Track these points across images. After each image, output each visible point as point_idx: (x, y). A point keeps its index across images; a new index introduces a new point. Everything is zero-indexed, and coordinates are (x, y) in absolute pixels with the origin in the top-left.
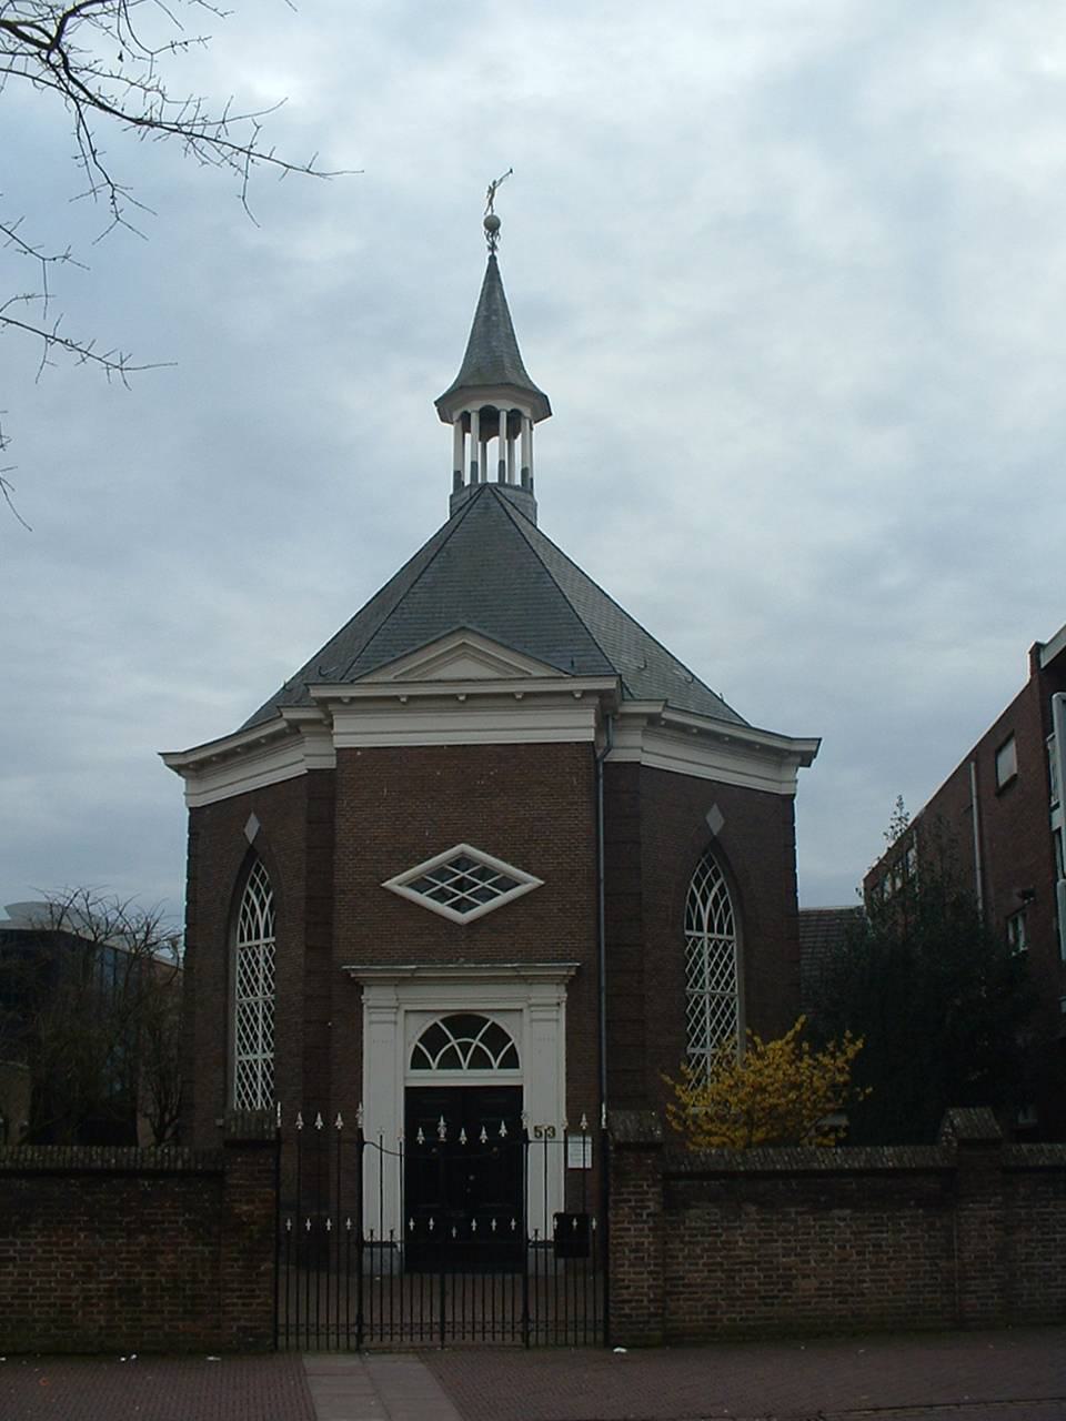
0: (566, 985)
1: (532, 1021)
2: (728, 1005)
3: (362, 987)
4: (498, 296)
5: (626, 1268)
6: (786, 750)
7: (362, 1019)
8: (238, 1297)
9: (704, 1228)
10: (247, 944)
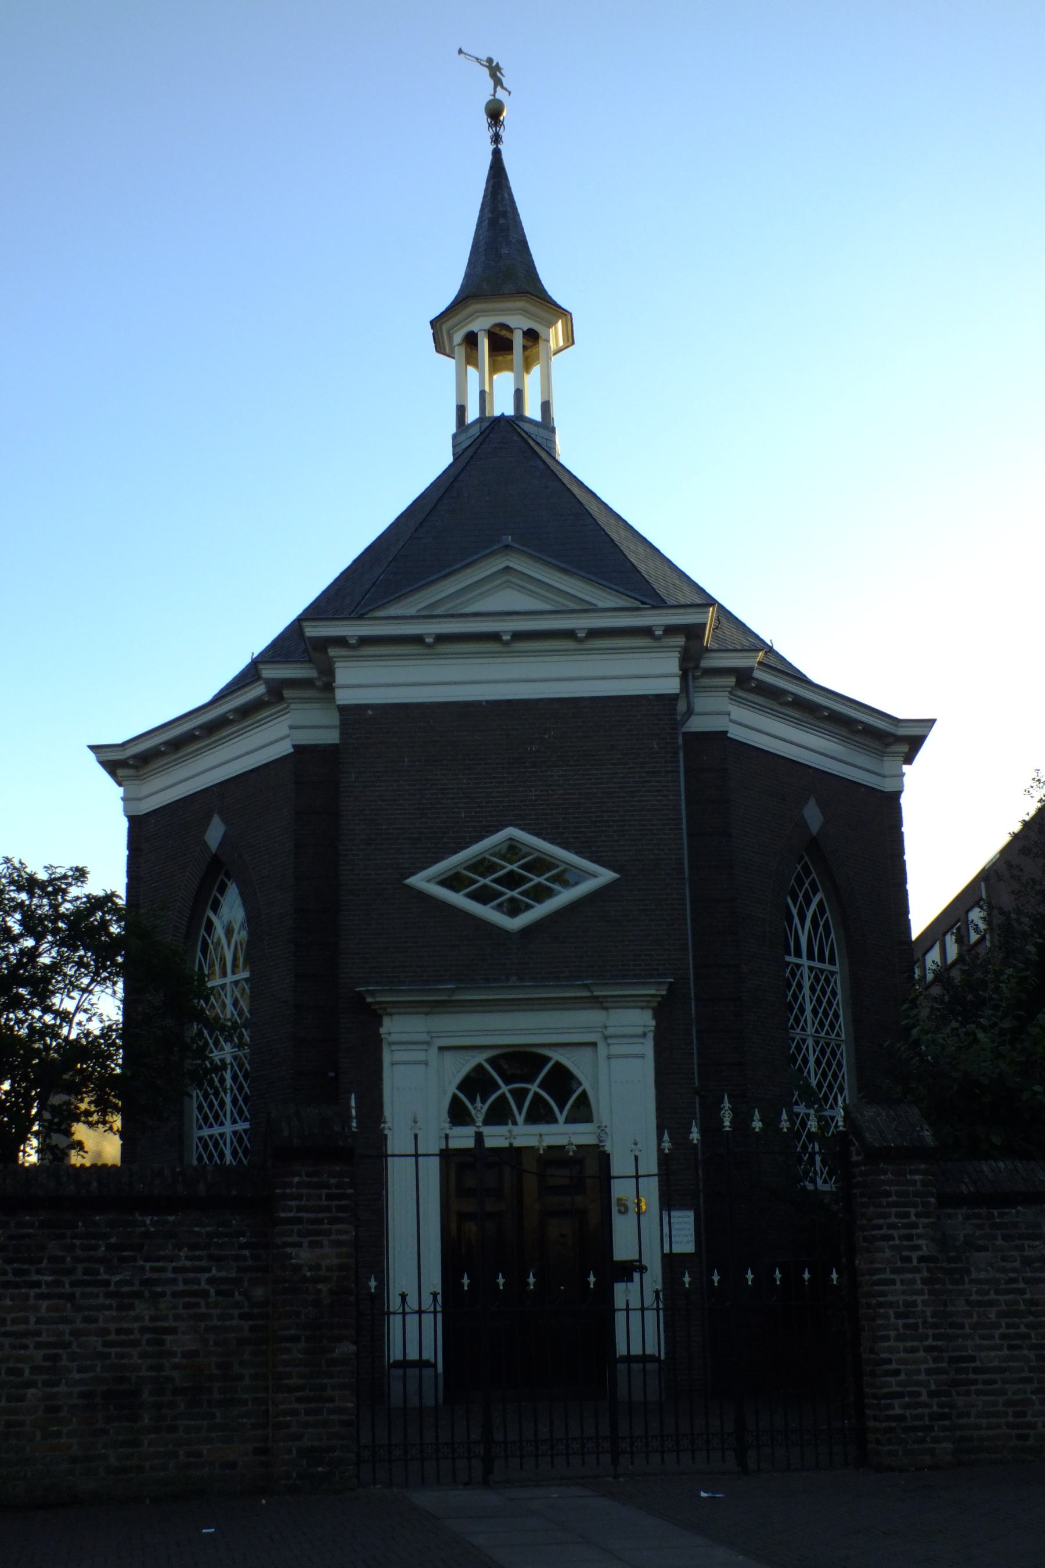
0: (653, 1009)
1: (609, 1058)
2: (834, 1054)
5: (892, 1343)
8: (299, 1400)
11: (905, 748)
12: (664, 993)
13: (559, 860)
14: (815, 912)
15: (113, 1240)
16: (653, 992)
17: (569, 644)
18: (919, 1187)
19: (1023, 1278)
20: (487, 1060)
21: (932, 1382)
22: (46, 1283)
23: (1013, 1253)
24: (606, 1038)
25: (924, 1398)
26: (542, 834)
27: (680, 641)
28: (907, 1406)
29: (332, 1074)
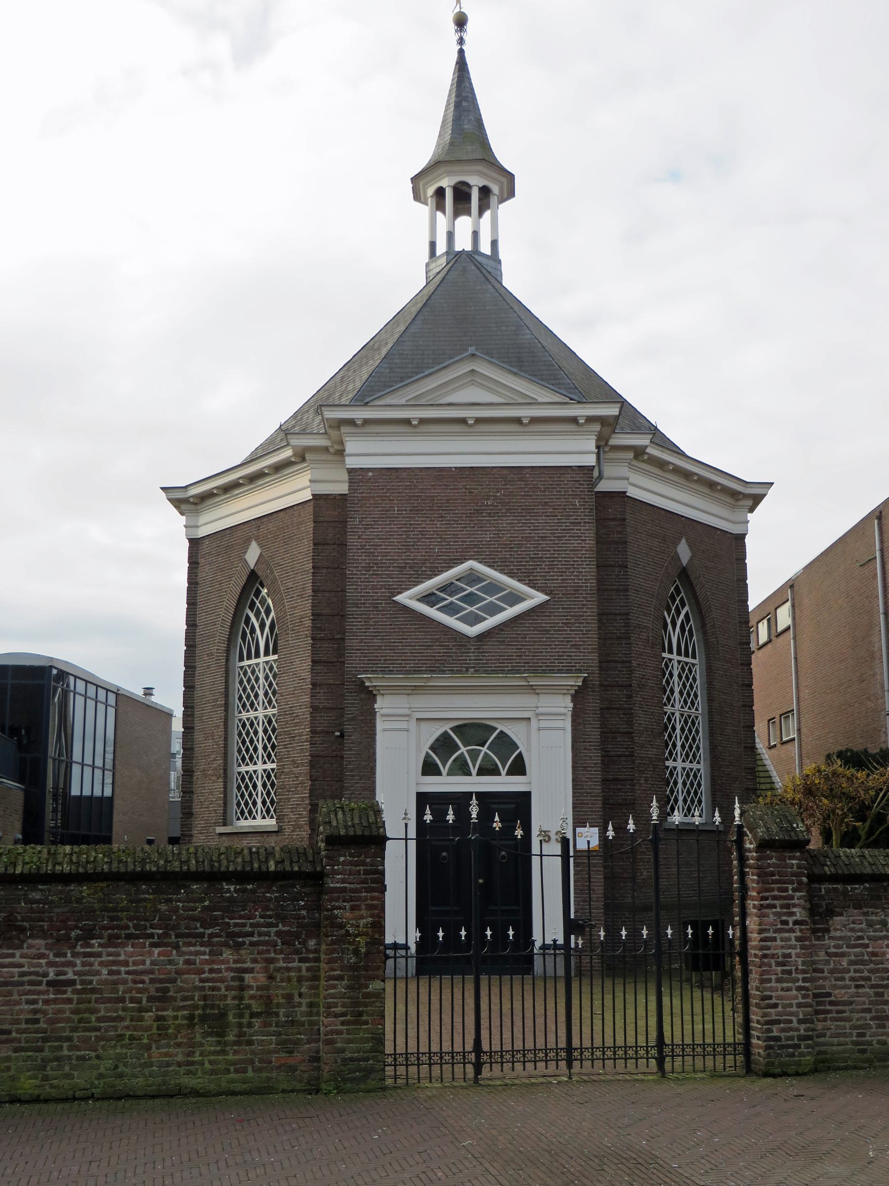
2: (693, 723)
3: (375, 695)
4: (468, 85)
5: (773, 984)
6: (740, 493)
7: (375, 727)
8: (343, 1023)
9: (850, 938)
10: (246, 663)
11: (750, 503)
12: (580, 684)
14: (682, 621)
15: (206, 903)
16: (573, 683)
17: (515, 428)
18: (795, 868)
19: (867, 936)
21: (801, 1012)
22: (158, 934)
23: (860, 918)
25: (795, 1024)
26: (493, 566)
27: (597, 427)
28: (783, 1030)
29: (338, 734)
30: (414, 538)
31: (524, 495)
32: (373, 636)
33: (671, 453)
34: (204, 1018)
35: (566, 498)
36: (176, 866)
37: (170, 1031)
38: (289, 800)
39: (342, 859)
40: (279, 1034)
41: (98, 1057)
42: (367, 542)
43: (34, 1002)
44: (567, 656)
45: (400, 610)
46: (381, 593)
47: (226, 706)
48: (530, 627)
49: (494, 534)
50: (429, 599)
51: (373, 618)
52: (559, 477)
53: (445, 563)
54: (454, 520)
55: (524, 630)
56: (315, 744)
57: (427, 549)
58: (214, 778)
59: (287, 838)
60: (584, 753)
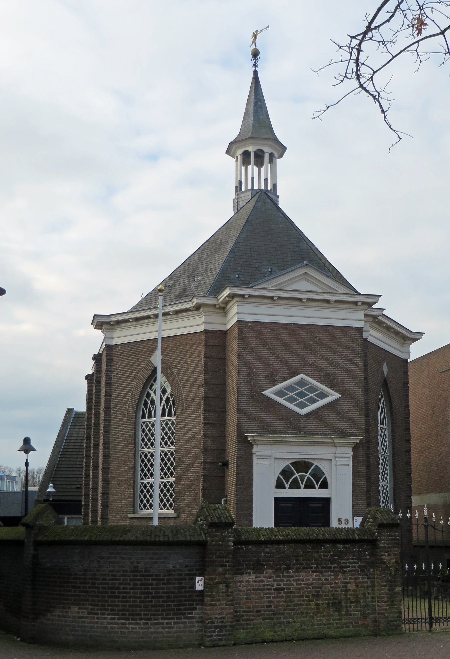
3: (253, 445)
6: (408, 337)
10: (147, 420)
12: (359, 442)
13: (319, 388)
15: (332, 553)
20: (291, 464)
22: (314, 567)
24: (336, 457)
26: (313, 378)
30: (273, 361)
31: (329, 341)
32: (251, 412)
33: (386, 318)
34: (333, 604)
35: (350, 344)
36: (321, 537)
37: (321, 610)
38: (184, 499)
39: (384, 533)
40: (361, 611)
41: (295, 622)
42: (248, 361)
43: (270, 597)
44: (350, 427)
45: (265, 399)
46: (256, 389)
47: (135, 444)
48: (331, 411)
49: (313, 361)
50: (280, 394)
51: (252, 403)
52: (346, 332)
53: (289, 375)
54: (293, 352)
55: (328, 413)
56: (206, 469)
57: (279, 367)
58: (126, 486)
59: (183, 521)
60: (358, 478)
